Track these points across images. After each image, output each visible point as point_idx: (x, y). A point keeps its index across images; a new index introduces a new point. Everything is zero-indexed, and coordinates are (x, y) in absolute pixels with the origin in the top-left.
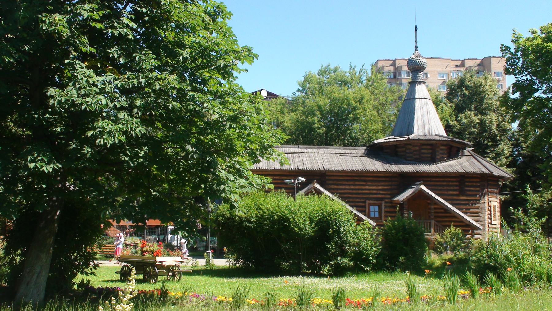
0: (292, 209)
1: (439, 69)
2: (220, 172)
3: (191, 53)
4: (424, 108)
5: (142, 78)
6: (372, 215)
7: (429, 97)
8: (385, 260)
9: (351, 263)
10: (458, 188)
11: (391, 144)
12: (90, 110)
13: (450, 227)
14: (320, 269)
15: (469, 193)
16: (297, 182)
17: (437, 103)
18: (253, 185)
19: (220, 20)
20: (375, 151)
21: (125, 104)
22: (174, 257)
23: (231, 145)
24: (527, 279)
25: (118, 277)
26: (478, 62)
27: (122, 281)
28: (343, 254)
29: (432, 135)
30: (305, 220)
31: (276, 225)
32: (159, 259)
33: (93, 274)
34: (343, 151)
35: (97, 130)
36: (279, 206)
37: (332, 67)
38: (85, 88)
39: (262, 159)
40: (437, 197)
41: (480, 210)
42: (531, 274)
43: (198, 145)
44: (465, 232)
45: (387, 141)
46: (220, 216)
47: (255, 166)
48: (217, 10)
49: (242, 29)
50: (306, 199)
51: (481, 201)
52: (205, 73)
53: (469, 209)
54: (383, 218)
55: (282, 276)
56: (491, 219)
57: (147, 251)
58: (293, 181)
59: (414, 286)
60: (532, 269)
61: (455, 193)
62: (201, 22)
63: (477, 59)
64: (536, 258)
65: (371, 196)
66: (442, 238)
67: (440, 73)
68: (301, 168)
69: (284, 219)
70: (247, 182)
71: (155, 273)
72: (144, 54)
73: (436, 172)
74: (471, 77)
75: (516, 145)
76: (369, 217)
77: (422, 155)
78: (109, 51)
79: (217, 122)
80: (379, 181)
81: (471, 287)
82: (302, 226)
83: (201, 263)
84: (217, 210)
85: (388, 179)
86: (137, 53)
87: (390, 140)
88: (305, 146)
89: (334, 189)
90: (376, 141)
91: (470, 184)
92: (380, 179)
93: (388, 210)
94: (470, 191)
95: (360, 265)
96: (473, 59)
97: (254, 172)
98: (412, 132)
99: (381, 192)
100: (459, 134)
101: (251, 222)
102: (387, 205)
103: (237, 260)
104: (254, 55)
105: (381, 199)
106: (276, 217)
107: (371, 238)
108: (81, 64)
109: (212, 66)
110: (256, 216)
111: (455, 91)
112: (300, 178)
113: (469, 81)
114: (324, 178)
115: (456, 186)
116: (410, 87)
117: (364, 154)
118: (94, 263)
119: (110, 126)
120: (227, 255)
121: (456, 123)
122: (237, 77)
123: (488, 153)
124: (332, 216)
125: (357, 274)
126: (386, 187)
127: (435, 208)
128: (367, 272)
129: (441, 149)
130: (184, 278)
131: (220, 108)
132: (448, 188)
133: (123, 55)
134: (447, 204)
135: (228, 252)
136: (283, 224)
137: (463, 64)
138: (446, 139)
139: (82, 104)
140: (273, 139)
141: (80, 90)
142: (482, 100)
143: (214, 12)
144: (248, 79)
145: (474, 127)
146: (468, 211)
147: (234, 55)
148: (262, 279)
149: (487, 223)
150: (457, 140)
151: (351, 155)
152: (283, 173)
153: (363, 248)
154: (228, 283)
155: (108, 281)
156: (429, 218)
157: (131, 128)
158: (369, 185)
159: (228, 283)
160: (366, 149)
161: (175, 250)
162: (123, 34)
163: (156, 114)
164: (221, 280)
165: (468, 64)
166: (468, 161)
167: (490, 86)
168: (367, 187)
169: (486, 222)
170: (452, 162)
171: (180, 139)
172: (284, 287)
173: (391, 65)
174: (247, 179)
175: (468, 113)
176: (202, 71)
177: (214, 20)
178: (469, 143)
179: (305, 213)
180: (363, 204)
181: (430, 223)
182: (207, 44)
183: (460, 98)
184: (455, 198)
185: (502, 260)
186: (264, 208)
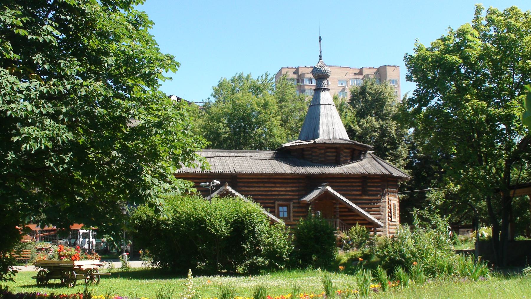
0: (208, 211)
1: (339, 77)
2: (146, 176)
3: (116, 60)
4: (329, 113)
5: (68, 84)
6: (281, 215)
7: (333, 103)
8: (298, 258)
9: (267, 262)
10: (360, 188)
11: (298, 147)
12: (16, 116)
13: (355, 225)
14: (235, 269)
15: (371, 193)
16: (212, 185)
17: (341, 109)
18: (176, 189)
19: (141, 28)
20: (283, 154)
21: (51, 110)
22: (92, 261)
23: (155, 149)
24: (430, 272)
25: (34, 281)
26: (375, 70)
27: (38, 285)
28: (258, 253)
29: (336, 139)
30: (220, 222)
31: (193, 227)
32: (77, 263)
33: (12, 279)
34: (253, 155)
35: (23, 136)
36: (195, 209)
37: (245, 75)
38: (10, 94)
39: (183, 165)
40: (342, 197)
41: (381, 209)
42: (433, 268)
43: (124, 150)
44: (369, 229)
45: (294, 144)
46: (136, 219)
47: (177, 171)
48: (138, 19)
49: (165, 36)
50: (221, 201)
51: (382, 201)
52: (129, 81)
53: (371, 208)
54: (292, 219)
55: (199, 276)
56: (391, 217)
57: (64, 255)
58: (208, 184)
59: (330, 282)
60: (435, 262)
61: (358, 193)
62: (125, 31)
63: (373, 68)
64: (439, 253)
65: (280, 197)
66: (348, 235)
67: (339, 81)
68: (213, 171)
69: (200, 221)
70: (170, 186)
71: (73, 277)
72: (69, 61)
73: (341, 174)
74: (372, 84)
75: (413, 148)
76: (279, 217)
77: (328, 158)
78: (34, 58)
79: (142, 127)
80: (287, 183)
81: (381, 281)
82: (218, 227)
83: (117, 265)
84: (133, 213)
85: (295, 181)
86: (62, 59)
87: (298, 144)
88: (217, 150)
89: (244, 191)
90: (284, 145)
91: (372, 184)
92: (289, 181)
93: (296, 210)
94: (372, 191)
95: (275, 262)
96: (370, 68)
97: (178, 176)
98: (317, 136)
99: (290, 193)
100: (360, 138)
101: (167, 225)
102: (295, 205)
103: (154, 263)
104: (176, 63)
105: (290, 200)
106: (192, 219)
107: (284, 237)
108: (5, 70)
109: (137, 73)
110: (173, 219)
111: (358, 97)
112: (215, 181)
113: (370, 89)
114: (235, 180)
115: (359, 186)
116: (315, 93)
117: (272, 157)
118: (12, 269)
119: (36, 132)
120: (143, 257)
121: (358, 128)
122: (161, 85)
123: (387, 156)
124: (247, 217)
125: (272, 272)
126: (294, 189)
127: (340, 208)
128: (281, 269)
129: (345, 152)
130: (102, 281)
131: (144, 114)
132: (352, 188)
133: (48, 62)
134: (351, 203)
135: (143, 254)
136: (199, 226)
137: (361, 72)
138: (349, 142)
139: (7, 110)
140: (195, 145)
141: (5, 97)
142: (382, 105)
143: (136, 20)
144: (172, 86)
145: (375, 131)
146: (370, 210)
147: (158, 63)
148: (180, 280)
149: (387, 221)
150: (359, 143)
151: (260, 159)
152: (196, 177)
153: (277, 247)
154: (147, 284)
155: (24, 287)
156: (335, 217)
157: (58, 134)
158: (278, 187)
159: (147, 284)
160: (274, 153)
161: (93, 254)
162: (48, 41)
163: (82, 120)
164: (140, 282)
165: (366, 72)
166: (369, 163)
167: (389, 93)
168: (277, 189)
169: (387, 219)
170: (355, 164)
171: (105, 146)
172: (203, 286)
173: (294, 73)
174: (170, 183)
175: (369, 118)
176: (125, 78)
177: (136, 27)
178: (370, 146)
179: (221, 215)
180: (273, 205)
181: (336, 222)
182: (131, 53)
183: (362, 104)
184: (358, 197)
185: (409, 255)
186: (180, 211)
